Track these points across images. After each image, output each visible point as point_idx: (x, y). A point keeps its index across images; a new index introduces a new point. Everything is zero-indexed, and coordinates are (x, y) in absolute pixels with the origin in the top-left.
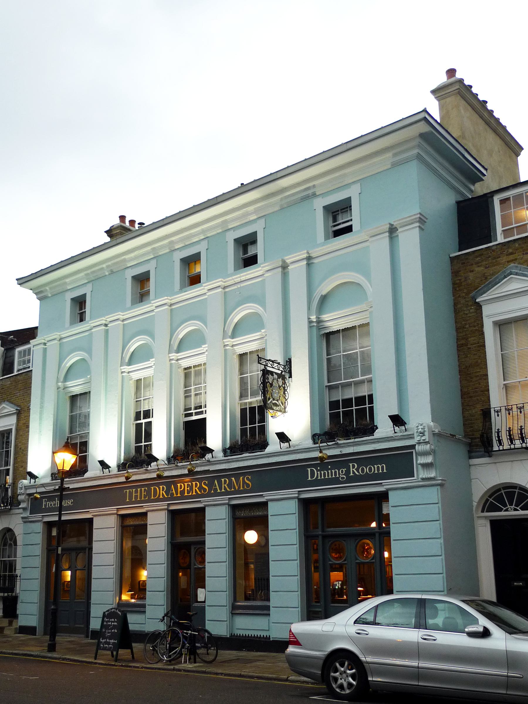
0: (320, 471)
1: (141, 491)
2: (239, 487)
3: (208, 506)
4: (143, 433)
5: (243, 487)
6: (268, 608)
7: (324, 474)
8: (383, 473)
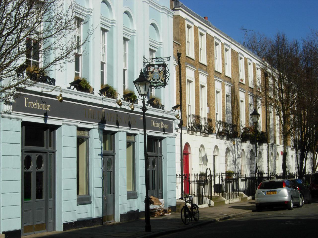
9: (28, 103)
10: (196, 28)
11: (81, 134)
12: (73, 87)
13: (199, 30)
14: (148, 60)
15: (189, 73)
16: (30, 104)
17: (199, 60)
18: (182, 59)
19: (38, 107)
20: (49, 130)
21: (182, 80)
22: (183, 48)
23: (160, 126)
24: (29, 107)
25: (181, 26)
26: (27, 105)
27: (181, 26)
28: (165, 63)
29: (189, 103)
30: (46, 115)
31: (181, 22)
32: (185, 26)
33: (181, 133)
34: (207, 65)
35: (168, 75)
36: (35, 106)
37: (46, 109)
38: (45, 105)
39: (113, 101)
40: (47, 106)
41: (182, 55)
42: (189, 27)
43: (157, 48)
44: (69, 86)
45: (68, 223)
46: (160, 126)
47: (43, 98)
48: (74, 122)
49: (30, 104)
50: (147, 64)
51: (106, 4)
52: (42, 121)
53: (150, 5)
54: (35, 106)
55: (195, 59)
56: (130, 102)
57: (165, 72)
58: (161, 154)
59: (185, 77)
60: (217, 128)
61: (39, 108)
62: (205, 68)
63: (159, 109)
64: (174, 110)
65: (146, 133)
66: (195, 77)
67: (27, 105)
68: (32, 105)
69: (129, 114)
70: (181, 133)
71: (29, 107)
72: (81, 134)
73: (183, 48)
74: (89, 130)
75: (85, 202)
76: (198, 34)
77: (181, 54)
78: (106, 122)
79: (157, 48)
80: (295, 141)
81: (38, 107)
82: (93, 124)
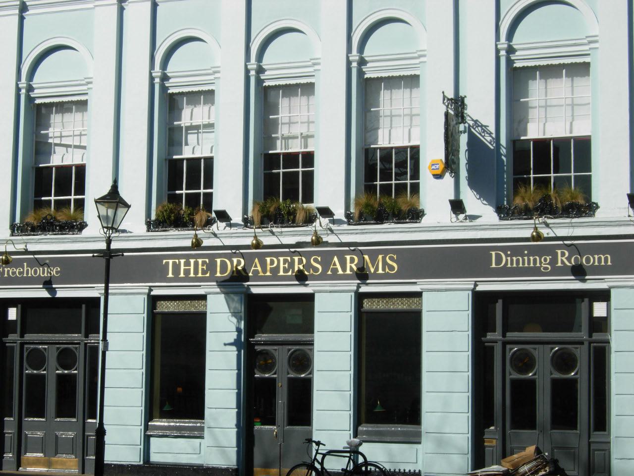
0: (511, 256)
1: (196, 264)
2: (377, 269)
3: (614, 287)
4: (131, 232)
5: (384, 269)
6: (202, 429)
7: (518, 261)
8: (599, 266)
9: (513, 259)
20: (586, 300)
24: (6, 275)
30: (48, 284)
36: (20, 273)
37: (49, 275)
38: (46, 269)
39: (33, 239)
40: (50, 269)
43: (589, 55)
45: (114, 464)
47: (364, 250)
48: (340, 286)
52: (44, 294)
56: (274, 223)
61: (30, 275)
65: (108, 292)
68: (14, 273)
69: (36, 258)
71: (6, 275)
74: (203, 297)
75: (412, 439)
78: (587, 273)
79: (589, 55)
80: (292, 203)
82: (200, 286)
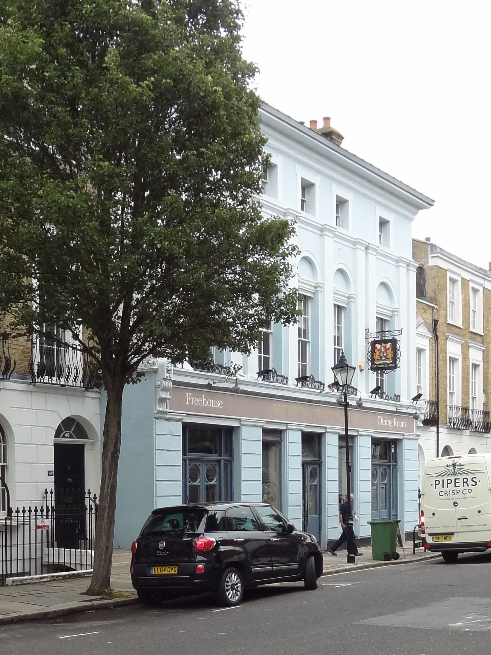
10: (465, 282)
11: (269, 438)
12: (374, 395)
13: (471, 285)
14: (373, 334)
15: (453, 348)
16: (194, 400)
17: (469, 328)
18: (441, 327)
19: (205, 404)
21: (441, 358)
22: (442, 312)
23: (393, 424)
25: (440, 281)
26: (190, 401)
27: (440, 281)
28: (396, 337)
29: (453, 390)
31: (440, 274)
32: (446, 279)
33: (438, 432)
34: (483, 334)
35: (399, 354)
36: (201, 403)
41: (441, 321)
42: (453, 281)
44: (370, 394)
46: (393, 424)
49: (194, 400)
50: (370, 340)
51: (310, 264)
53: (377, 256)
54: (201, 403)
55: (462, 327)
57: (395, 350)
58: (396, 462)
59: (446, 353)
60: (477, 418)
62: (480, 339)
63: (390, 401)
64: (415, 402)
66: (463, 353)
67: (190, 401)
70: (438, 432)
72: (269, 438)
73: (444, 312)
76: (469, 290)
77: (438, 321)
81: (205, 404)
